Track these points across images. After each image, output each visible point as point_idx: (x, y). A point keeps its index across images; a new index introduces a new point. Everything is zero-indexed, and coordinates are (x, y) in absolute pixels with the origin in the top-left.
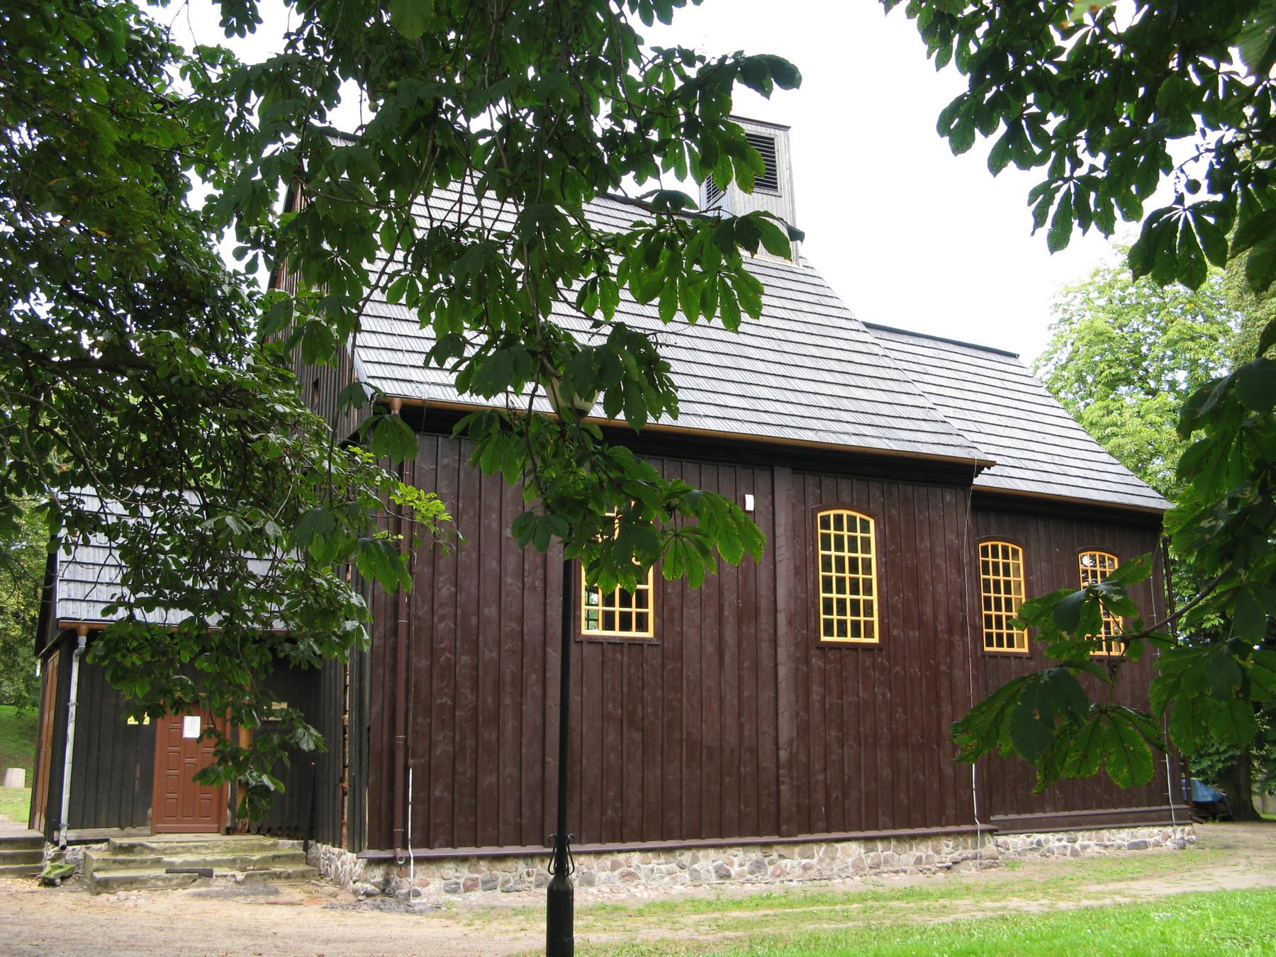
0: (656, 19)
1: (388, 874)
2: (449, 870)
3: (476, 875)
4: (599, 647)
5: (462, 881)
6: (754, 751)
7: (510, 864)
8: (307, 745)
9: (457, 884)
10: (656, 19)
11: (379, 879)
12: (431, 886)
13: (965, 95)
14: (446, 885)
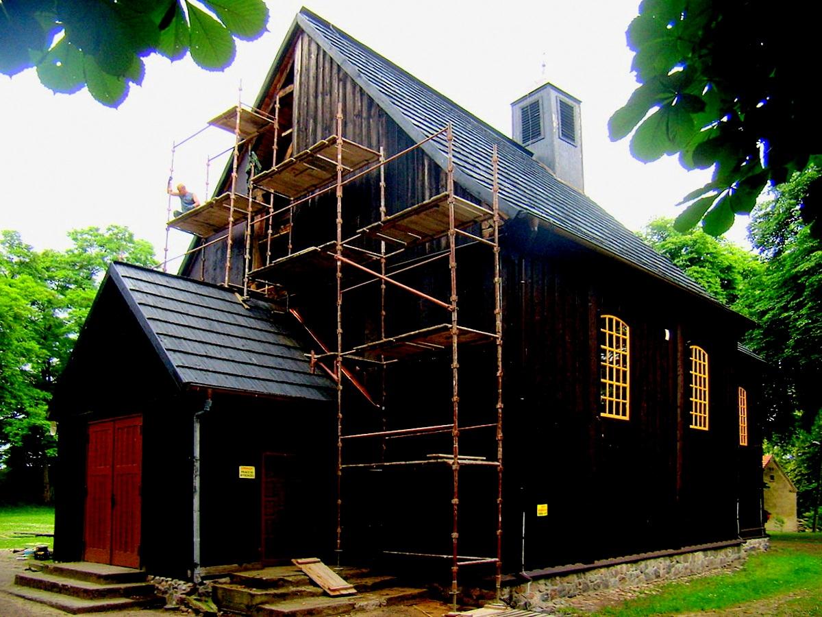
1: (511, 591)
3: (555, 587)
11: (506, 596)
12: (535, 598)
14: (543, 595)
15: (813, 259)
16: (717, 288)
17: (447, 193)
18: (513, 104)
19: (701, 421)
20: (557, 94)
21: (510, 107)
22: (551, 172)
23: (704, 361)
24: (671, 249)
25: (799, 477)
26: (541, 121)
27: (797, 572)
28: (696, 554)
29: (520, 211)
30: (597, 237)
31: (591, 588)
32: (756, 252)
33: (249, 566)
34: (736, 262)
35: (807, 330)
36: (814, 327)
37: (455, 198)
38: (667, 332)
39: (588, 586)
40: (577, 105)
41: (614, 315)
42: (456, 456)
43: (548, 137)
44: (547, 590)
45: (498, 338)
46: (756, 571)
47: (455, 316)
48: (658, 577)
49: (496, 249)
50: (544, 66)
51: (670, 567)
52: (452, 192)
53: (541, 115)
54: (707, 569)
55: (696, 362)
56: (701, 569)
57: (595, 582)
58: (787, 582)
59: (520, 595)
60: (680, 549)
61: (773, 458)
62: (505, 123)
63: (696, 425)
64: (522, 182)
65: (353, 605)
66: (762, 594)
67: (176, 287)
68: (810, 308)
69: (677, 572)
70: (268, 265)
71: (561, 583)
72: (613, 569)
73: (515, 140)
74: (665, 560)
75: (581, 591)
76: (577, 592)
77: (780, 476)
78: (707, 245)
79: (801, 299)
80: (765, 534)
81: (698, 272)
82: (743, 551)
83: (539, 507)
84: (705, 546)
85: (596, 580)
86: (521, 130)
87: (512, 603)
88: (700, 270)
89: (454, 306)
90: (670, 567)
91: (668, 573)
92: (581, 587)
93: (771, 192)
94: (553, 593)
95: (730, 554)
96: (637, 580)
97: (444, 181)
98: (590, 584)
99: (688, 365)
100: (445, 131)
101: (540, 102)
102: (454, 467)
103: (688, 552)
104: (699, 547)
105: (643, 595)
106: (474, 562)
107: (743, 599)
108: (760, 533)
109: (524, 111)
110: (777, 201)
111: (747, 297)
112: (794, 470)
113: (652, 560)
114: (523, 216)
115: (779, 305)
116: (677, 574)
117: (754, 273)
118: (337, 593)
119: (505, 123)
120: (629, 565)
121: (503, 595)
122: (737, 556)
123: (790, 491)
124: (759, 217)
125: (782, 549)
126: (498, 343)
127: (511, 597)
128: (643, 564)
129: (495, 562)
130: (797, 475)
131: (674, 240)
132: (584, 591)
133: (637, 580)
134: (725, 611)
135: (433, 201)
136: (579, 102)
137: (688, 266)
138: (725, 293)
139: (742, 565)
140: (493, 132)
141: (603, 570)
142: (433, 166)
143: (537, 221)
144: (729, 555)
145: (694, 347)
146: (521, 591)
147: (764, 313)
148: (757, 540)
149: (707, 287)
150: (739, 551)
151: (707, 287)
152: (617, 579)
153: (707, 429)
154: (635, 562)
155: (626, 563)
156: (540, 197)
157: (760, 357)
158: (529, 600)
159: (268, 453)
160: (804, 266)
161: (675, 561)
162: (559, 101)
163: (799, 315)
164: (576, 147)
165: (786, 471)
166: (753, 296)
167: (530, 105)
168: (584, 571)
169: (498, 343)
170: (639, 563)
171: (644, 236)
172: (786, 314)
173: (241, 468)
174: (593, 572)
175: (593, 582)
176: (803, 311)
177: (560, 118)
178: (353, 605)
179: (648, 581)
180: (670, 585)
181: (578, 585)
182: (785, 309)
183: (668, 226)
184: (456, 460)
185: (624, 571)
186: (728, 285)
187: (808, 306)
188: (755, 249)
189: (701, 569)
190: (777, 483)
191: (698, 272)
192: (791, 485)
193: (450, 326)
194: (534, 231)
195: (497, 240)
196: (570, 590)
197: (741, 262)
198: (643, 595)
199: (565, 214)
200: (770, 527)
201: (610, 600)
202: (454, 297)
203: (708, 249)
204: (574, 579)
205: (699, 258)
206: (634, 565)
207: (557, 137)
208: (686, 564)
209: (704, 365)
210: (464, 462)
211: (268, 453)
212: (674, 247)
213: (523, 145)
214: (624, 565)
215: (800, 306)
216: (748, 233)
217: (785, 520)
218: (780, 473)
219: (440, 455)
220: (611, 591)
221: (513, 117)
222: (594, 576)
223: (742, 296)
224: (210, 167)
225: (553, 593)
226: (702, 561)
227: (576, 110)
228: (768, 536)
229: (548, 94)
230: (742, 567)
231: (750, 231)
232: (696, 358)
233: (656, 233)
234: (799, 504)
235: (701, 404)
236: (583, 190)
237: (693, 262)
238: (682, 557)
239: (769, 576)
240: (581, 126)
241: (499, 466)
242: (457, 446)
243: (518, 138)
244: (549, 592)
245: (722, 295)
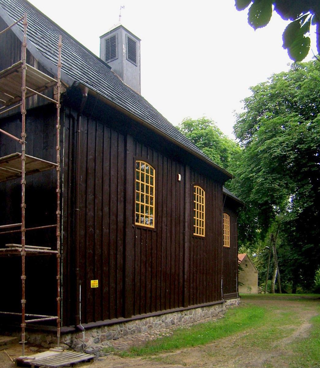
0: (247, 10)
1: (72, 338)
2: (94, 332)
3: (104, 334)
4: (140, 230)
5: (100, 337)
6: (179, 275)
7: (115, 327)
8: (80, 281)
9: (98, 339)
10: (247, 10)
11: (68, 341)
12: (90, 341)
13: (285, 75)
14: (95, 340)
15: (265, 145)
16: (218, 161)
17: (21, 61)
18: (101, 37)
19: (201, 231)
20: (126, 33)
21: (99, 39)
22: (121, 79)
23: (203, 196)
24: (195, 137)
25: (260, 265)
26: (116, 49)
27: (250, 318)
28: (197, 309)
29: (75, 81)
30: (139, 114)
31: (129, 333)
32: (238, 140)
34: (228, 147)
35: (262, 184)
36: (266, 182)
37: (27, 66)
38: (180, 176)
39: (127, 332)
40: (138, 41)
41: (145, 161)
42: (23, 246)
43: (120, 57)
44: (98, 336)
45: (58, 166)
46: (230, 318)
47: (24, 147)
48: (173, 324)
49: (58, 106)
50: (120, 16)
51: (180, 319)
52: (25, 61)
53: (117, 45)
54: (204, 318)
55: (198, 196)
56: (200, 318)
57: (132, 329)
58: (244, 324)
59: (78, 340)
60: (187, 307)
61: (247, 256)
62: (96, 48)
63: (197, 233)
64: (92, 74)
66: (229, 333)
68: (264, 172)
69: (185, 321)
70: (136, 191)
71: (108, 331)
72: (144, 321)
73: (102, 59)
74: (178, 314)
75: (123, 335)
76: (120, 336)
77: (250, 265)
78: (213, 136)
79: (259, 167)
80: (239, 296)
81: (208, 151)
82: (224, 307)
83: (92, 282)
84: (202, 305)
85: (133, 328)
86: (105, 53)
87: (73, 345)
88: (209, 149)
89: (23, 140)
90: (180, 319)
91: (180, 321)
93: (246, 108)
94: (103, 338)
95: (217, 309)
96: (160, 327)
97: (32, 62)
98: (128, 331)
99: (193, 197)
100: (23, 19)
101: (116, 37)
102: (22, 253)
103: (192, 309)
104: (199, 305)
105: (161, 337)
106: (39, 320)
107: (218, 337)
108: (235, 296)
109: (107, 42)
110: (249, 112)
111: (233, 166)
112: (258, 261)
113: (170, 315)
114: (77, 84)
115: (248, 170)
116: (185, 322)
117: (237, 153)
119: (96, 48)
120: (155, 318)
121: (66, 341)
122: (221, 309)
123: (255, 273)
124: (240, 122)
125: (247, 304)
126: (57, 170)
127: (72, 342)
128: (163, 317)
129: (56, 320)
130: (259, 264)
131: (196, 132)
132: (125, 335)
133: (160, 327)
134: (205, 346)
135: (13, 68)
136: (139, 40)
137: (203, 147)
138: (222, 164)
139: (224, 315)
140: (87, 51)
141: (137, 322)
143: (87, 90)
144: (216, 309)
145: (197, 187)
146: (79, 337)
147: (240, 175)
148: (234, 300)
149: (213, 159)
150: (222, 307)
151: (213, 159)
152: (147, 326)
153: (204, 236)
154: (159, 315)
155: (153, 316)
156: (104, 85)
157: (239, 199)
158: (85, 343)
160: (261, 148)
161: (184, 314)
163: (258, 176)
164: (137, 66)
165: (254, 262)
166: (236, 165)
167: (110, 38)
169: (57, 170)
170: (161, 316)
171: (181, 129)
172: (251, 175)
174: (131, 323)
176: (260, 174)
177: (127, 47)
179: (167, 327)
180: (179, 330)
181: (120, 331)
182: (251, 172)
183: (193, 124)
184: (24, 249)
185: (151, 321)
186: (224, 159)
187: (263, 171)
188: (238, 139)
189: (200, 318)
190: (249, 268)
191: (208, 151)
192: (256, 269)
193: (20, 154)
194: (85, 96)
195: (59, 100)
196: (115, 335)
197: (231, 147)
198: (161, 337)
199: (118, 96)
200: (242, 291)
201: (139, 341)
202: (24, 134)
203: (214, 138)
204: (118, 327)
205: (209, 143)
206: (158, 318)
207: (126, 58)
208: (191, 316)
209: (203, 198)
210: (29, 250)
212: (196, 136)
213: (106, 62)
214: (151, 318)
215: (259, 171)
216: (234, 130)
217: (252, 287)
218: (250, 263)
219: (14, 245)
220: (142, 335)
221: (100, 45)
222: (131, 326)
223: (230, 165)
225: (103, 338)
226: (201, 314)
227: (137, 44)
228: (240, 297)
229: (121, 32)
230: (223, 316)
231: (235, 129)
232: (198, 193)
233: (187, 128)
234: (259, 279)
235: (200, 221)
236: (140, 93)
237: (205, 145)
238: (188, 312)
239: (236, 321)
240: (140, 54)
241: (58, 253)
242: (24, 238)
243: (103, 58)
244: (100, 337)
245: (221, 164)
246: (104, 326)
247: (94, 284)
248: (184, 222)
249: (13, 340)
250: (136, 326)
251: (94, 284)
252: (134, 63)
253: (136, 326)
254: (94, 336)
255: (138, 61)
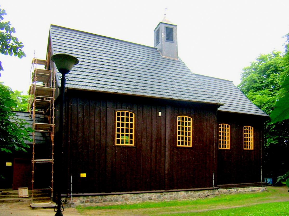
1: (66, 199)
7: (97, 197)
12: (77, 202)
14: (81, 202)
33: (8, 189)
65: (20, 201)
67: (150, 72)
72: (121, 196)
92: (102, 200)
118: (21, 197)
136: (176, 26)
142: (157, 44)
159: (15, 159)
162: (157, 29)
168: (105, 195)
173: (7, 163)
175: (109, 199)
178: (20, 201)
211: (15, 159)
214: (129, 195)
224: (166, 15)
227: (174, 29)
240: (177, 34)
246: (89, 196)
247: (83, 175)
248: (165, 139)
249: (48, 198)
250: (114, 198)
251: (83, 175)
252: (171, 42)
253: (114, 198)
254: (80, 200)
255: (174, 39)
